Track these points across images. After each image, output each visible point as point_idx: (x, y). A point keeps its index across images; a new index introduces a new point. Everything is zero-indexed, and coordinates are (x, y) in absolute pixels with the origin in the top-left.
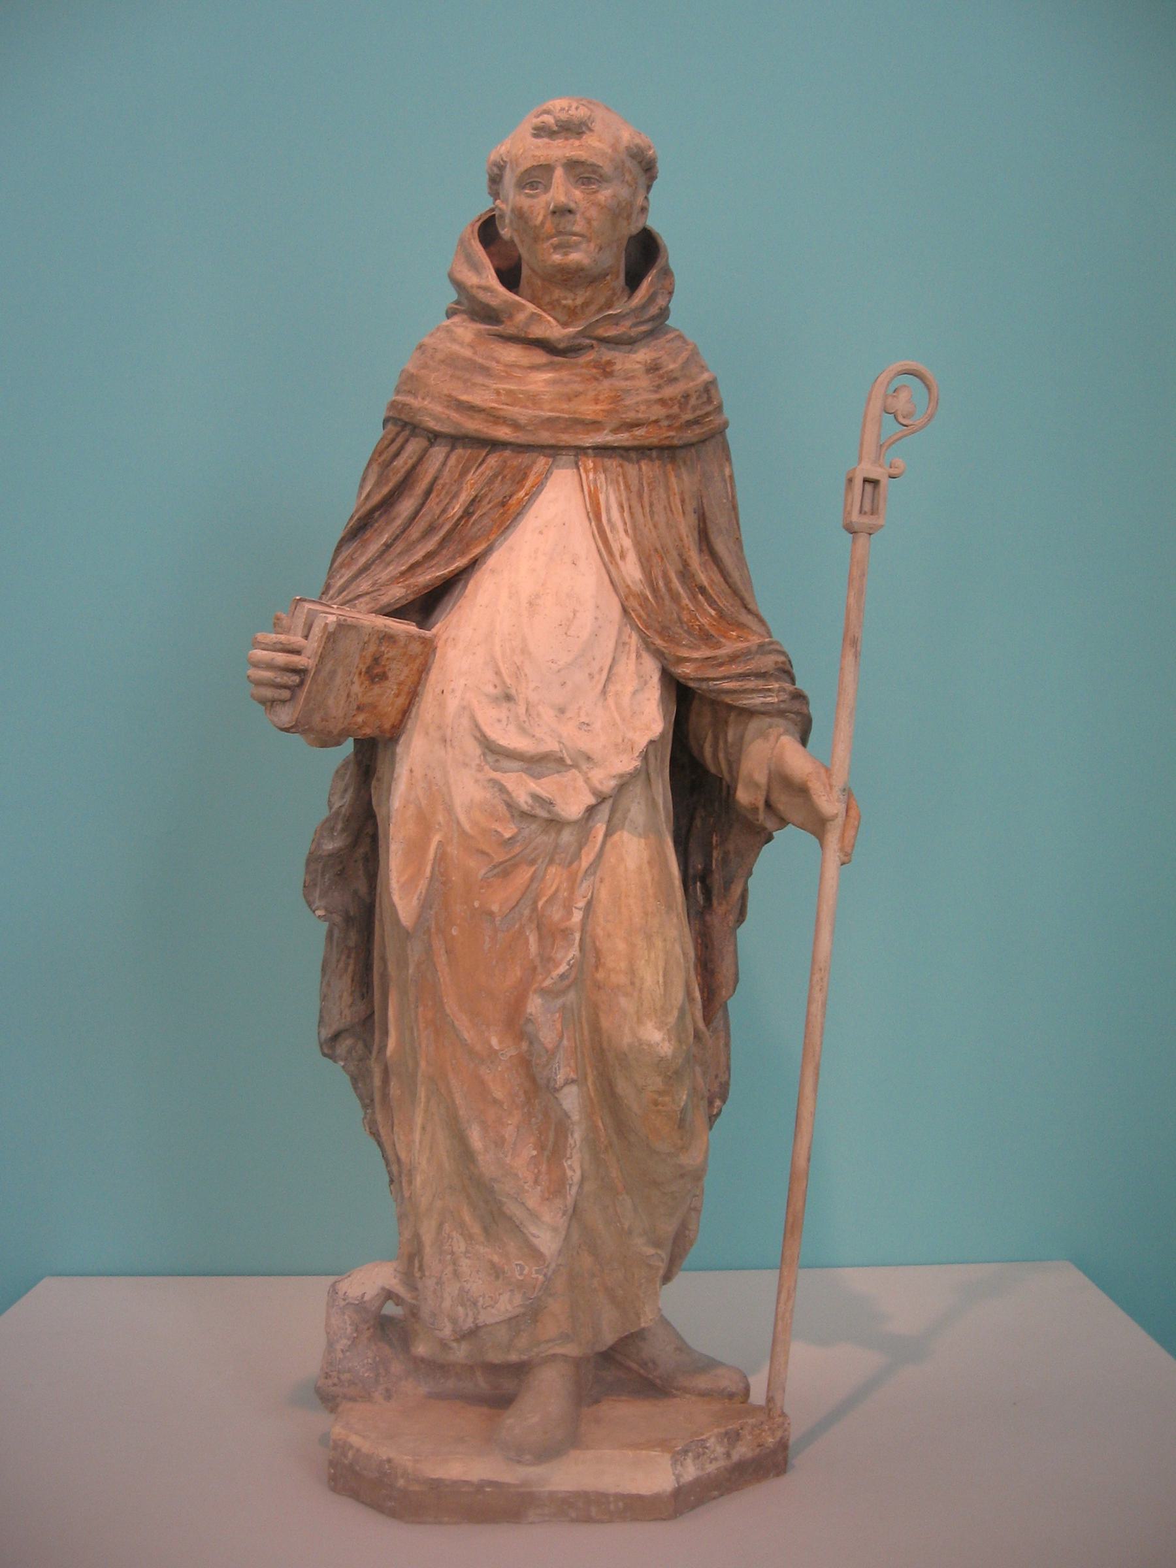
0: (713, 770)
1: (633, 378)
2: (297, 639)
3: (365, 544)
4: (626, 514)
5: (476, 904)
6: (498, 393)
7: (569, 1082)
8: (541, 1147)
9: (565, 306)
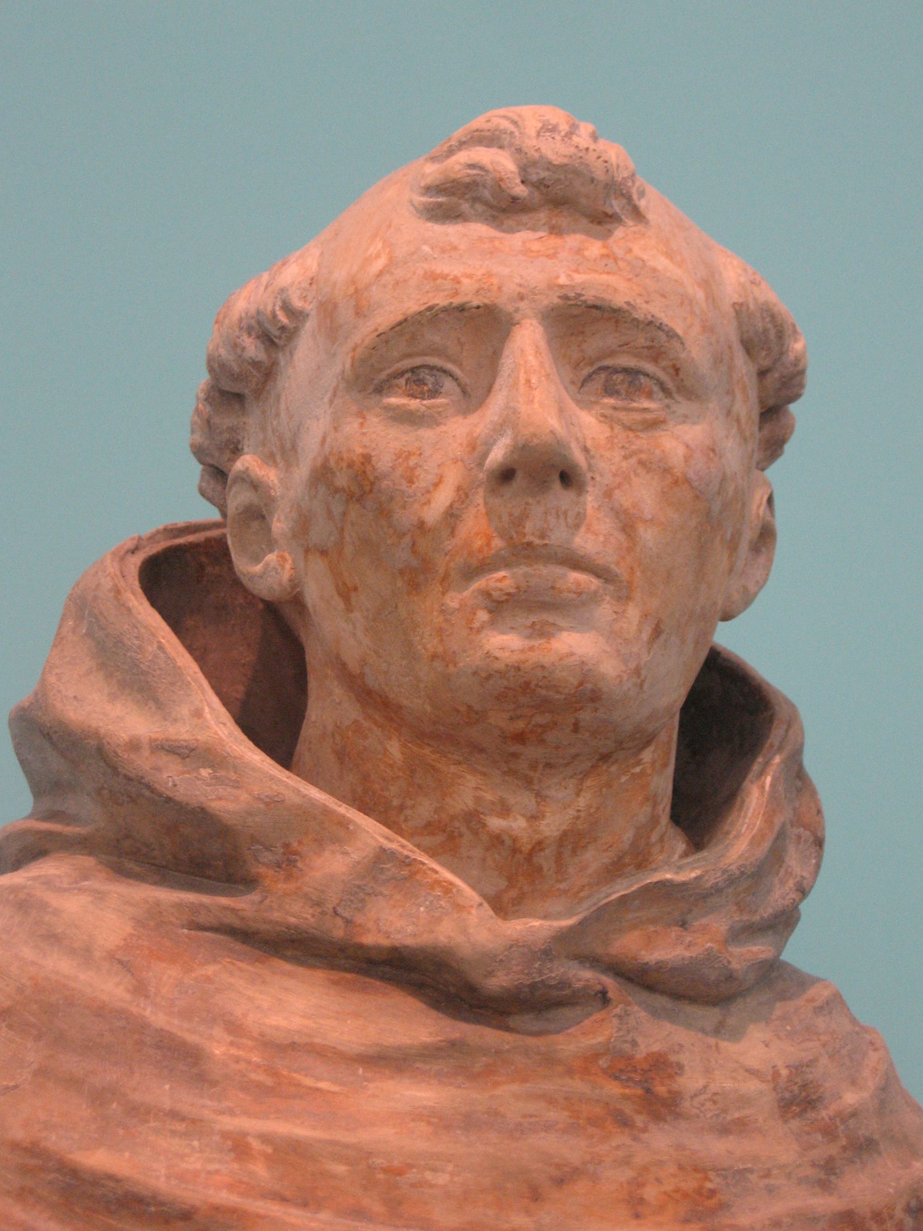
1: (740, 1127)
6: (239, 1147)
9: (497, 840)
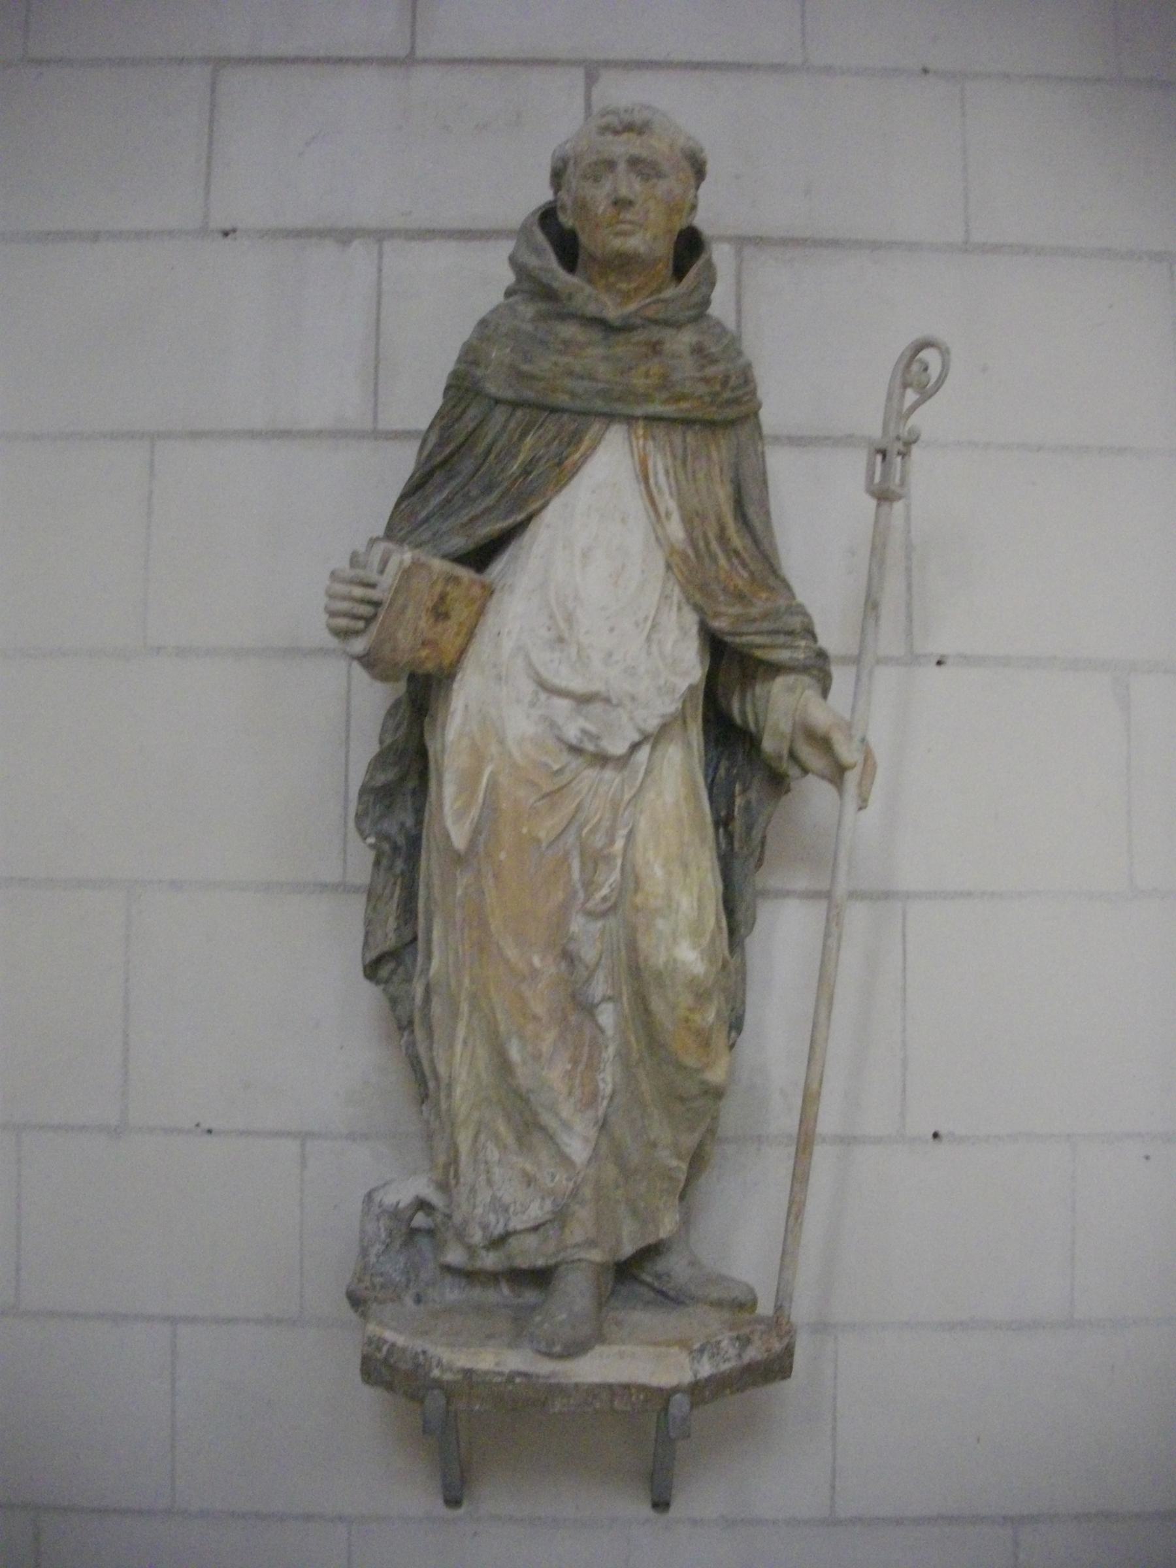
0: (738, 720)
2: (373, 576)
3: (426, 500)
4: (673, 482)
5: (525, 830)
7: (607, 999)
8: (575, 1062)
